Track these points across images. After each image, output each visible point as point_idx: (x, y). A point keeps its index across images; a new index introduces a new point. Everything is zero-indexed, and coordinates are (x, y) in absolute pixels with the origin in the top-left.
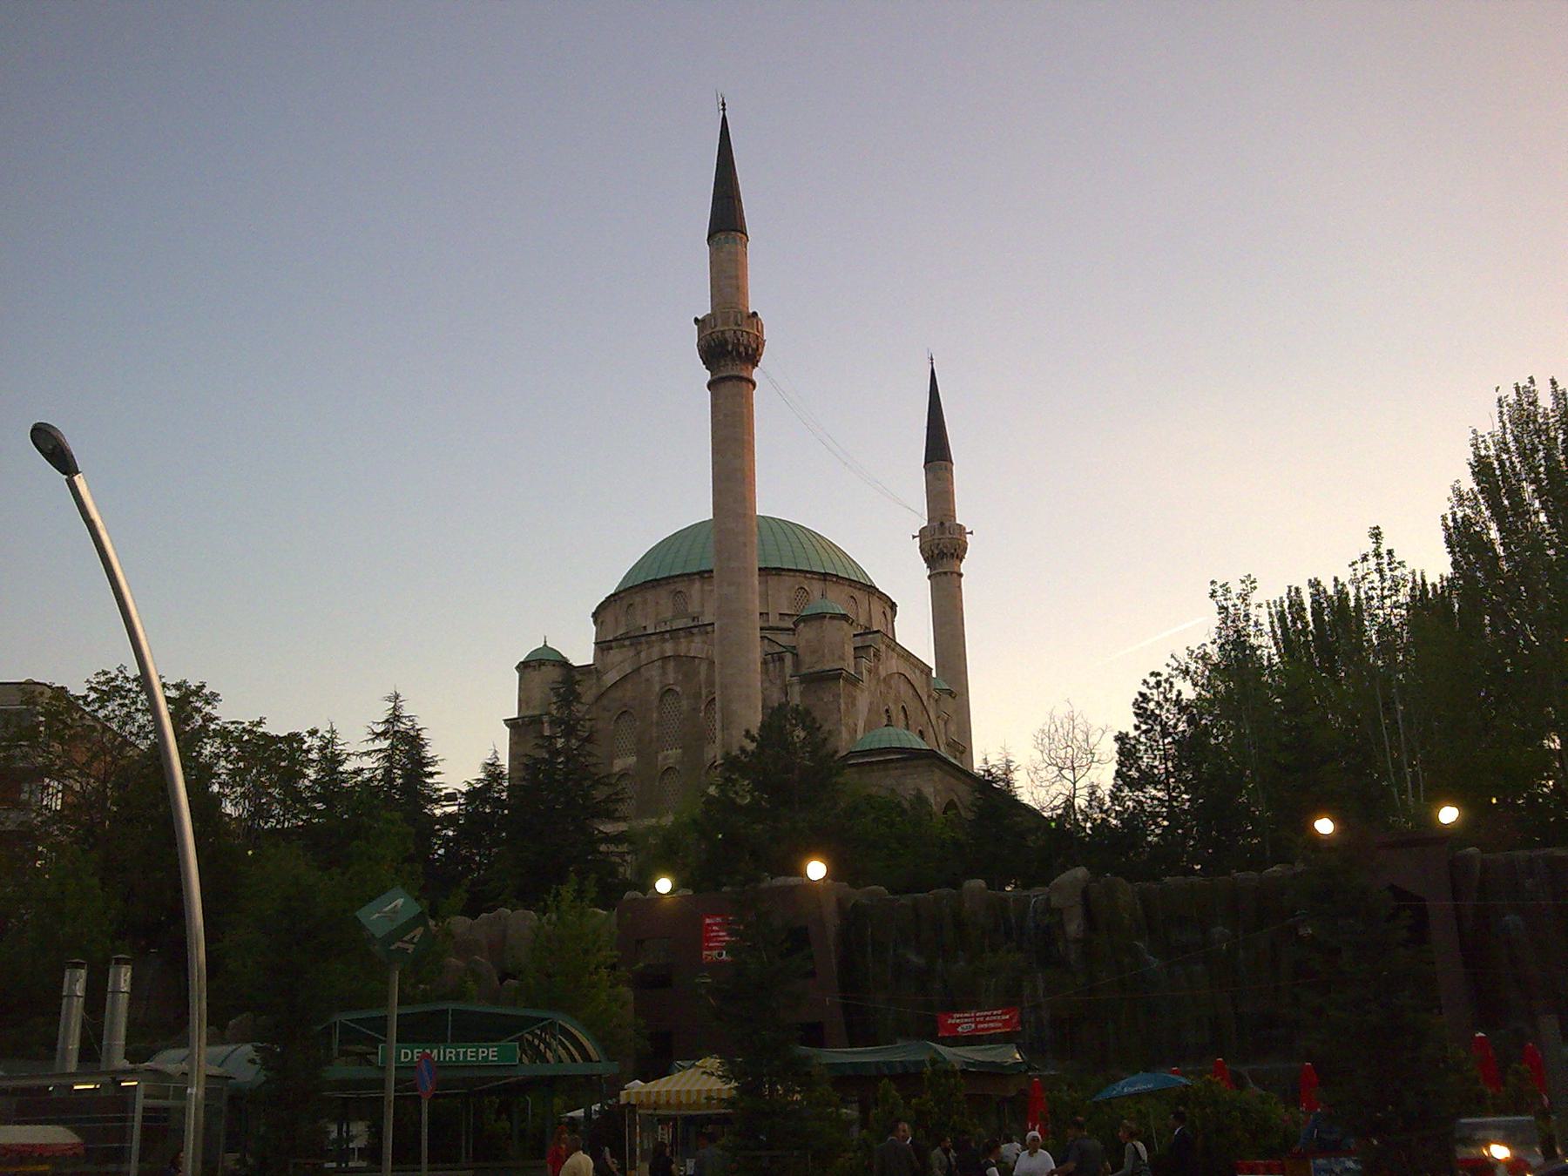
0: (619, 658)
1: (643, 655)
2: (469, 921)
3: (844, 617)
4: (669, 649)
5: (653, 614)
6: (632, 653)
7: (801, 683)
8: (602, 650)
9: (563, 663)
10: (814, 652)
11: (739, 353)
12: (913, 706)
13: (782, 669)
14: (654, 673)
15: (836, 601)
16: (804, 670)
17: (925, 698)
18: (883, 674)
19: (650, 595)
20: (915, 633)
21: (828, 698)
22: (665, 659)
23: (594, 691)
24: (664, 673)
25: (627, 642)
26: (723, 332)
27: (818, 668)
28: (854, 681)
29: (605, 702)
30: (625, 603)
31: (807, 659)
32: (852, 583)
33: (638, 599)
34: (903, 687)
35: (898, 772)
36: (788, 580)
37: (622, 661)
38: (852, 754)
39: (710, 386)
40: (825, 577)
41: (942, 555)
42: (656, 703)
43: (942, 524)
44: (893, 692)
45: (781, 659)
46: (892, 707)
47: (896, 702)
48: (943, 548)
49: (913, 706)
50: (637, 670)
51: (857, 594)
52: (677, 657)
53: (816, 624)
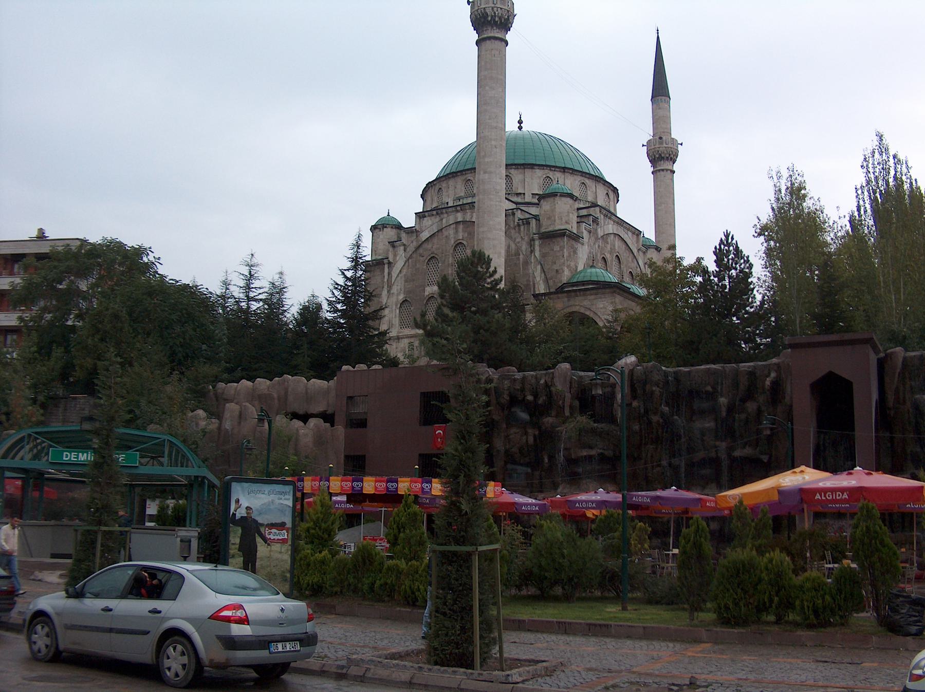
0: (430, 223)
1: (444, 221)
2: (268, 382)
3: (571, 196)
4: (460, 216)
5: (452, 193)
7: (540, 239)
8: (420, 218)
9: (399, 227)
10: (549, 218)
11: (496, 22)
12: (624, 255)
13: (529, 230)
14: (451, 231)
15: (570, 184)
16: (543, 230)
17: (635, 251)
18: (600, 233)
19: (451, 182)
20: (636, 208)
21: (557, 248)
22: (457, 223)
23: (415, 243)
25: (434, 212)
27: (551, 229)
28: (576, 238)
29: (421, 251)
30: (437, 187)
31: (544, 222)
32: (583, 174)
33: (444, 185)
34: (618, 243)
35: (593, 297)
36: (539, 173)
37: (430, 226)
38: (569, 284)
39: (478, 43)
40: (564, 170)
41: (661, 158)
42: (451, 251)
43: (661, 138)
44: (609, 247)
45: (528, 223)
46: (608, 256)
47: (611, 253)
48: (662, 155)
49: (624, 255)
50: (440, 231)
51: (587, 181)
52: (464, 222)
53: (552, 199)
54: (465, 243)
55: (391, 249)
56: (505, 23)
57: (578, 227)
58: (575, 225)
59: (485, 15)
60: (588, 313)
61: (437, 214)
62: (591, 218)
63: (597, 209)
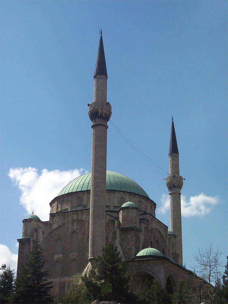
4: (75, 217)
6: (62, 217)
8: (52, 216)
11: (103, 116)
14: (70, 225)
16: (121, 227)
21: (129, 236)
22: (73, 221)
23: (49, 231)
24: (73, 225)
26: (97, 109)
41: (174, 186)
50: (64, 224)
52: (77, 220)
54: (78, 231)
55: (35, 233)
56: (107, 118)
57: (140, 225)
58: (138, 224)
59: (97, 112)
60: (150, 273)
61: (62, 214)
62: (146, 220)
63: (148, 215)
